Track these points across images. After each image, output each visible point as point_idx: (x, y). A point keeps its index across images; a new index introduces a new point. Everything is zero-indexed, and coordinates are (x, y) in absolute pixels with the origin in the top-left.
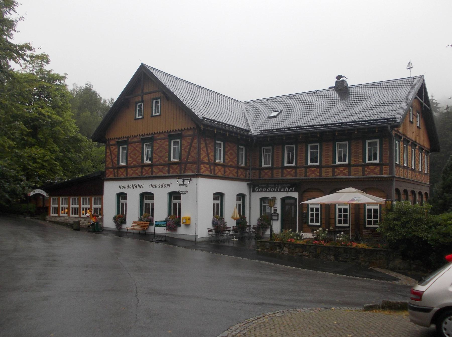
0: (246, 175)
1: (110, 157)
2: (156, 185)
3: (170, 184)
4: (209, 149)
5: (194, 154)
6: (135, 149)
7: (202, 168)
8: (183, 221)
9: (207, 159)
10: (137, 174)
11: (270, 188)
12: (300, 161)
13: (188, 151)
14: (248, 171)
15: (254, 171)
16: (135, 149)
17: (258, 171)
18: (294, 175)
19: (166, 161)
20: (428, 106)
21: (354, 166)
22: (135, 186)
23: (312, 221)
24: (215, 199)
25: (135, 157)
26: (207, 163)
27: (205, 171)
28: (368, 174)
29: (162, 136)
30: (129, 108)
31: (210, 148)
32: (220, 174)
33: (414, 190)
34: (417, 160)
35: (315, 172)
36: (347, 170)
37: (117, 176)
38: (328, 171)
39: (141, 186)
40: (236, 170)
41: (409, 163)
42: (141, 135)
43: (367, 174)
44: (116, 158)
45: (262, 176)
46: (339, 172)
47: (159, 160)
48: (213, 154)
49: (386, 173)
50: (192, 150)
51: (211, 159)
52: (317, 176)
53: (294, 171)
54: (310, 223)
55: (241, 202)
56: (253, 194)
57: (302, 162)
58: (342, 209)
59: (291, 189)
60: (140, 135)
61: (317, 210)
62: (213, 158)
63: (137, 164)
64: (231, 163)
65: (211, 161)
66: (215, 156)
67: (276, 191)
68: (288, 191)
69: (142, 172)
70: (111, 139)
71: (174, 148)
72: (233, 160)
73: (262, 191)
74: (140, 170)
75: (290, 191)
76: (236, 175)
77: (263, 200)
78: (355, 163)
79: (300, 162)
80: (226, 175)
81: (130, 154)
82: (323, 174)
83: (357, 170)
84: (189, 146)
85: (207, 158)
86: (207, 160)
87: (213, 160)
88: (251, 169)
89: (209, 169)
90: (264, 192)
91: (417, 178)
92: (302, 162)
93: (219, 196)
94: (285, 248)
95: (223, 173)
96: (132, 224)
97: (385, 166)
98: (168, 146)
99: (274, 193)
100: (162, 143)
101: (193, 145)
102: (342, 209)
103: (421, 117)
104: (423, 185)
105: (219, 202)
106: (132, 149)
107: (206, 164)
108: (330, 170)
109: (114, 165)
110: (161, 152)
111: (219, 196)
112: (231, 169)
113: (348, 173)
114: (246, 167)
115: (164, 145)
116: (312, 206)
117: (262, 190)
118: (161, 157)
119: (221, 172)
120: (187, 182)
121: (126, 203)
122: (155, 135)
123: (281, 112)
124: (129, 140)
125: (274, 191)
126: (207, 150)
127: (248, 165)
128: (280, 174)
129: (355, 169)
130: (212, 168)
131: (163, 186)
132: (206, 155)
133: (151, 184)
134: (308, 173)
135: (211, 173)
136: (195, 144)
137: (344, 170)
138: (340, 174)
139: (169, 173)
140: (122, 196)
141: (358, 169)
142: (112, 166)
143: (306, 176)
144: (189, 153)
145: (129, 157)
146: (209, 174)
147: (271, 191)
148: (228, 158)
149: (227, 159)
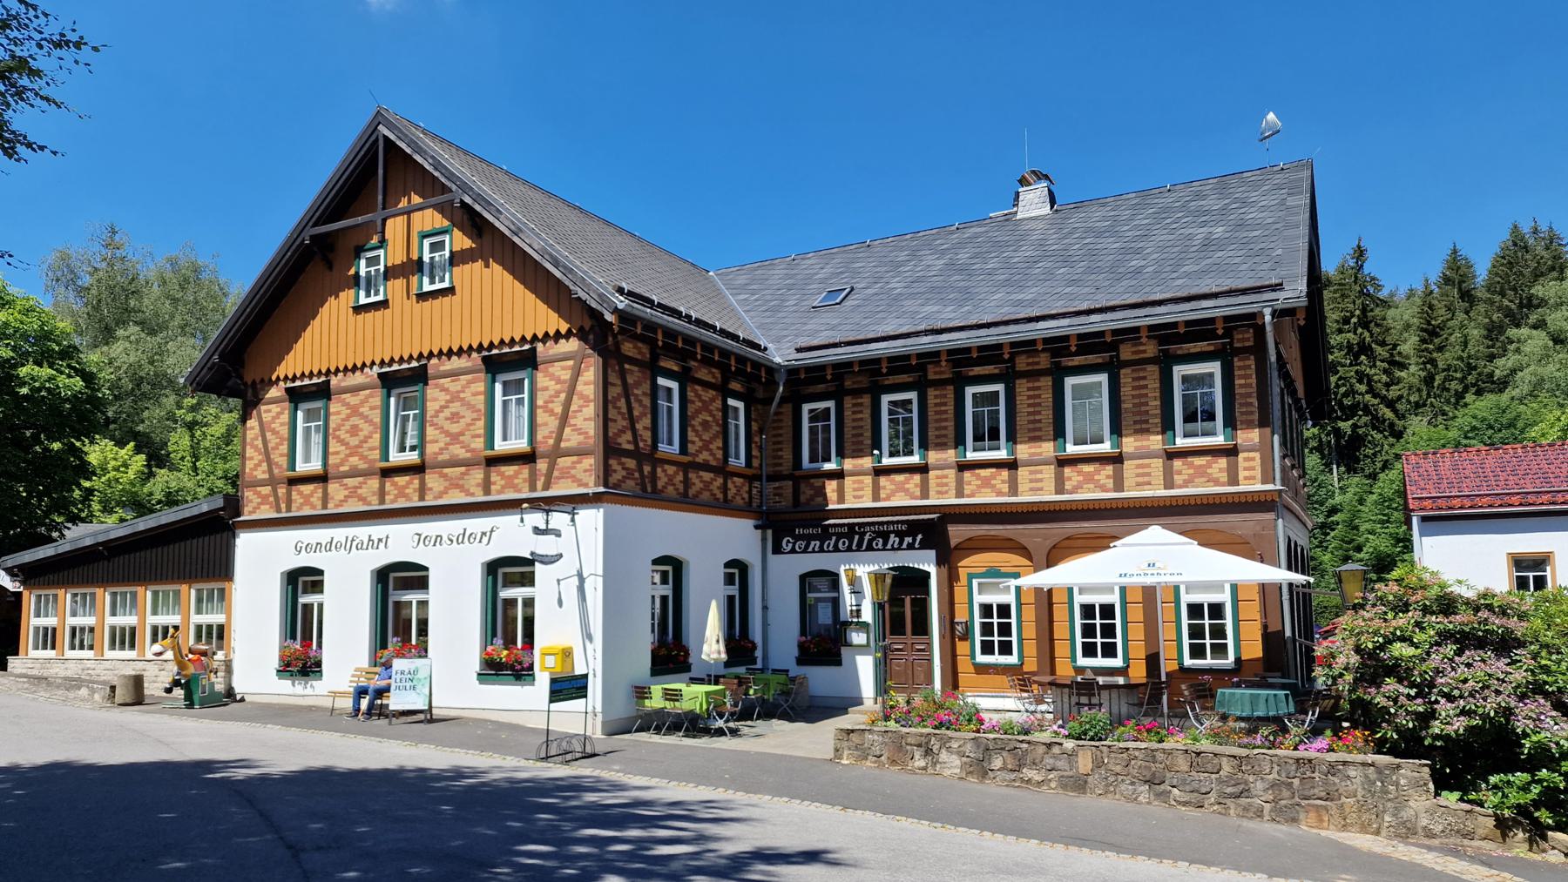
1: (259, 443)
2: (437, 536)
3: (492, 531)
4: (635, 405)
5: (585, 420)
6: (355, 411)
8: (543, 662)
9: (631, 439)
10: (363, 499)
11: (834, 538)
13: (559, 409)
14: (757, 484)
15: (777, 484)
16: (355, 411)
18: (918, 493)
19: (473, 451)
21: (1133, 457)
22: (355, 544)
26: (627, 454)
27: (624, 482)
28: (1185, 484)
29: (456, 363)
30: (330, 268)
31: (640, 402)
35: (993, 482)
36: (1111, 473)
37: (289, 509)
38: (1039, 476)
39: (380, 540)
40: (720, 481)
42: (377, 362)
43: (1181, 482)
44: (281, 447)
45: (803, 498)
46: (1081, 478)
47: (447, 449)
48: (647, 421)
49: (1253, 478)
50: (573, 407)
52: (999, 494)
56: (773, 559)
58: (1201, 606)
59: (908, 540)
60: (373, 363)
62: (647, 435)
63: (363, 466)
65: (641, 445)
66: (654, 429)
67: (854, 548)
68: (899, 549)
69: (382, 494)
71: (505, 403)
72: (711, 446)
73: (805, 551)
74: (378, 485)
75: (904, 546)
76: (720, 496)
77: (807, 581)
78: (1136, 448)
80: (690, 495)
81: (335, 430)
82: (1023, 485)
83: (1146, 470)
84: (563, 396)
85: (628, 436)
86: (629, 442)
87: (649, 442)
89: (637, 475)
90: (814, 551)
94: (944, 756)
96: (353, 676)
98: (482, 397)
99: (899, 552)
100: (459, 388)
101: (579, 387)
102: (1094, 606)
106: (345, 412)
108: (1049, 472)
109: (276, 471)
110: (455, 417)
111: (672, 569)
112: (707, 476)
113: (1112, 481)
115: (466, 395)
116: (1196, 598)
117: (807, 546)
118: (455, 438)
119: (674, 485)
120: (559, 519)
121: (321, 606)
122: (434, 361)
123: (852, 289)
125: (849, 549)
126: (630, 409)
127: (756, 463)
128: (868, 491)
129: (1138, 467)
130: (647, 469)
131: (333, 547)
132: (625, 423)
133: (420, 535)
134: (966, 487)
136: (586, 384)
138: (1085, 486)
139: (487, 492)
140: (303, 580)
141: (1148, 466)
142: (266, 476)
143: (960, 494)
144: (564, 419)
147: (836, 549)
148: (696, 439)
149: (693, 443)
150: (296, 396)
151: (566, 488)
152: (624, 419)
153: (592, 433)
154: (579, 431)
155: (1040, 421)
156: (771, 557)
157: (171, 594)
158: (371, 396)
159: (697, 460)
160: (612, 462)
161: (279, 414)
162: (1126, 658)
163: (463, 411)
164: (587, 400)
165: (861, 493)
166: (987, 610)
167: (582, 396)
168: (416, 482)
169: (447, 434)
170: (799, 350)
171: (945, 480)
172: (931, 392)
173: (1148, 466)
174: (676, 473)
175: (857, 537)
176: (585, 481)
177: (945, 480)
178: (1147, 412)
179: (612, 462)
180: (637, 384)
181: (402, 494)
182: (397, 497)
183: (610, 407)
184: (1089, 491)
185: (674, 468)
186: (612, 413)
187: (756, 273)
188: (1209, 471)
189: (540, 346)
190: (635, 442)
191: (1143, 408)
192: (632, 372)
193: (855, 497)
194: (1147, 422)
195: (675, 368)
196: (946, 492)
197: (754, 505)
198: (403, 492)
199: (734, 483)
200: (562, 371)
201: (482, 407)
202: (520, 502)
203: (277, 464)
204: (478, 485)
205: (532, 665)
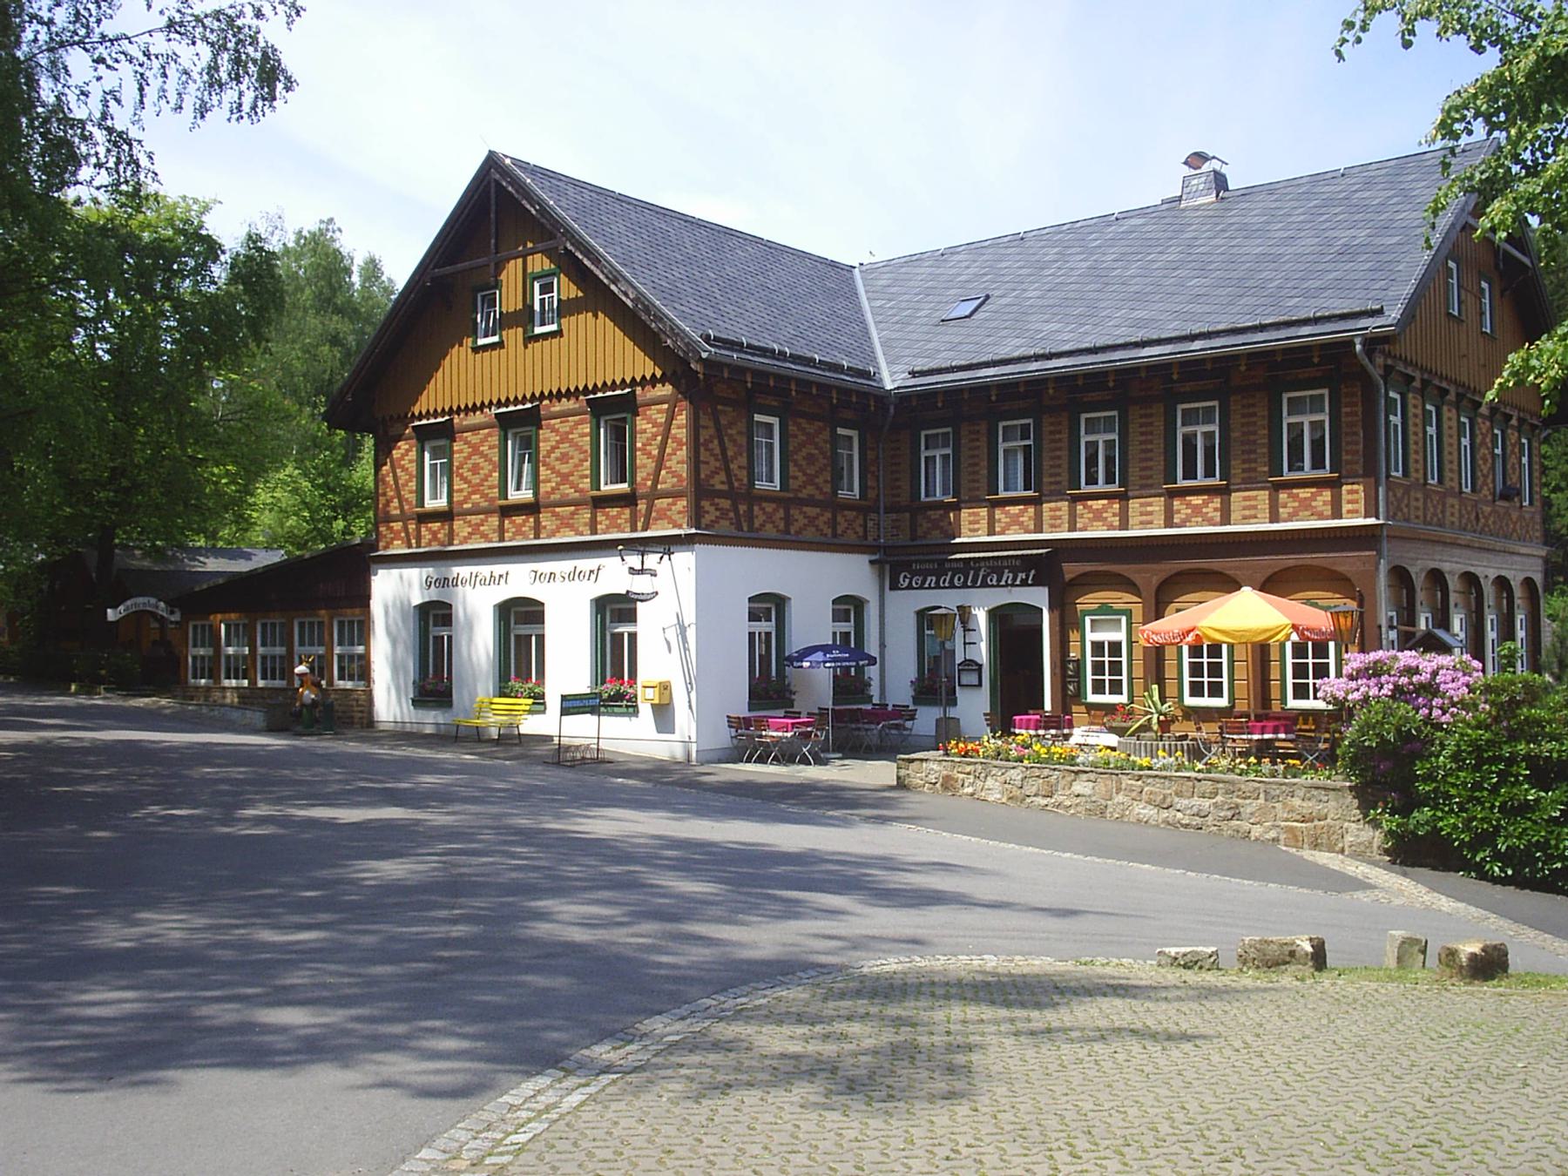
0: (865, 531)
6: (475, 450)
7: (708, 512)
12: (1051, 475)
13: (655, 452)
14: (873, 516)
15: (894, 516)
16: (475, 450)
17: (907, 515)
18: (1032, 527)
19: (581, 491)
20: (1524, 254)
23: (1098, 688)
24: (753, 617)
25: (476, 480)
29: (566, 404)
31: (734, 441)
32: (769, 530)
33: (1472, 569)
34: (1485, 461)
38: (1149, 509)
39: (501, 576)
40: (828, 515)
41: (1451, 470)
45: (919, 532)
48: (743, 461)
50: (668, 450)
51: (737, 480)
53: (1031, 510)
54: (1092, 698)
55: (848, 627)
56: (892, 597)
57: (1058, 479)
58: (1102, 643)
61: (1215, 650)
62: (743, 474)
64: (810, 490)
65: (736, 484)
66: (750, 468)
68: (1013, 585)
70: (391, 417)
73: (921, 587)
75: (1018, 582)
76: (829, 531)
77: (925, 618)
79: (1053, 480)
80: (792, 531)
81: (458, 468)
83: (1252, 503)
84: (659, 438)
85: (722, 476)
86: (723, 483)
87: (745, 481)
88: (882, 511)
89: (732, 515)
90: (930, 588)
91: (1486, 525)
92: (1058, 479)
93: (768, 607)
95: (782, 526)
97: (1349, 487)
100: (568, 429)
102: (1103, 643)
103: (1497, 294)
104: (1513, 553)
105: (768, 626)
106: (467, 450)
107: (719, 497)
110: (564, 458)
111: (768, 607)
112: (812, 511)
114: (863, 503)
117: (924, 582)
118: (565, 478)
119: (773, 522)
120: (652, 560)
122: (546, 402)
123: (988, 297)
124: (456, 420)
125: (965, 586)
126: (724, 450)
127: (871, 494)
128: (984, 524)
129: (1245, 499)
130: (742, 508)
135: (740, 528)
136: (679, 427)
137: (1206, 504)
141: (1255, 498)
144: (660, 462)
145: (456, 480)
146: (733, 531)
147: (952, 586)
149: (795, 478)
150: (423, 435)
151: (663, 529)
152: (717, 460)
153: (685, 475)
154: (674, 474)
155: (1151, 450)
156: (888, 593)
157: (534, 638)
158: (489, 435)
159: (800, 495)
160: (706, 504)
161: (408, 451)
162: (1232, 699)
163: (572, 451)
164: (680, 443)
165: (976, 526)
166: (1098, 647)
167: (675, 439)
168: (532, 520)
169: (559, 474)
170: (913, 374)
171: (1058, 513)
172: (1046, 420)
173: (1255, 498)
174: (775, 510)
175: (972, 572)
176: (679, 522)
177: (1058, 513)
178: (1254, 442)
179: (706, 504)
180: (731, 425)
181: (519, 532)
182: (515, 534)
183: (702, 449)
184: (1197, 524)
185: (774, 505)
186: (704, 455)
187: (903, 270)
188: (1314, 504)
189: (639, 389)
190: (730, 483)
191: (1252, 438)
192: (724, 412)
193: (970, 530)
194: (1254, 452)
195: (776, 404)
196: (1059, 526)
197: (870, 538)
198: (519, 533)
199: (844, 516)
200: (658, 414)
201: (588, 448)
202: (615, 542)
203: (407, 500)
204: (586, 525)
205: (636, 696)
